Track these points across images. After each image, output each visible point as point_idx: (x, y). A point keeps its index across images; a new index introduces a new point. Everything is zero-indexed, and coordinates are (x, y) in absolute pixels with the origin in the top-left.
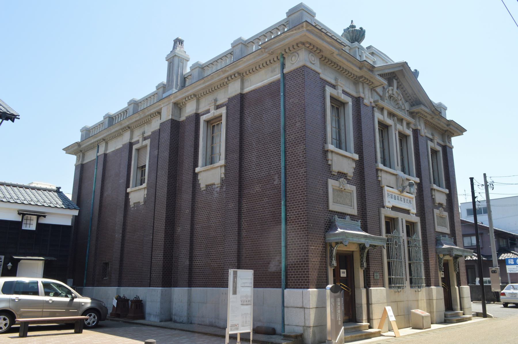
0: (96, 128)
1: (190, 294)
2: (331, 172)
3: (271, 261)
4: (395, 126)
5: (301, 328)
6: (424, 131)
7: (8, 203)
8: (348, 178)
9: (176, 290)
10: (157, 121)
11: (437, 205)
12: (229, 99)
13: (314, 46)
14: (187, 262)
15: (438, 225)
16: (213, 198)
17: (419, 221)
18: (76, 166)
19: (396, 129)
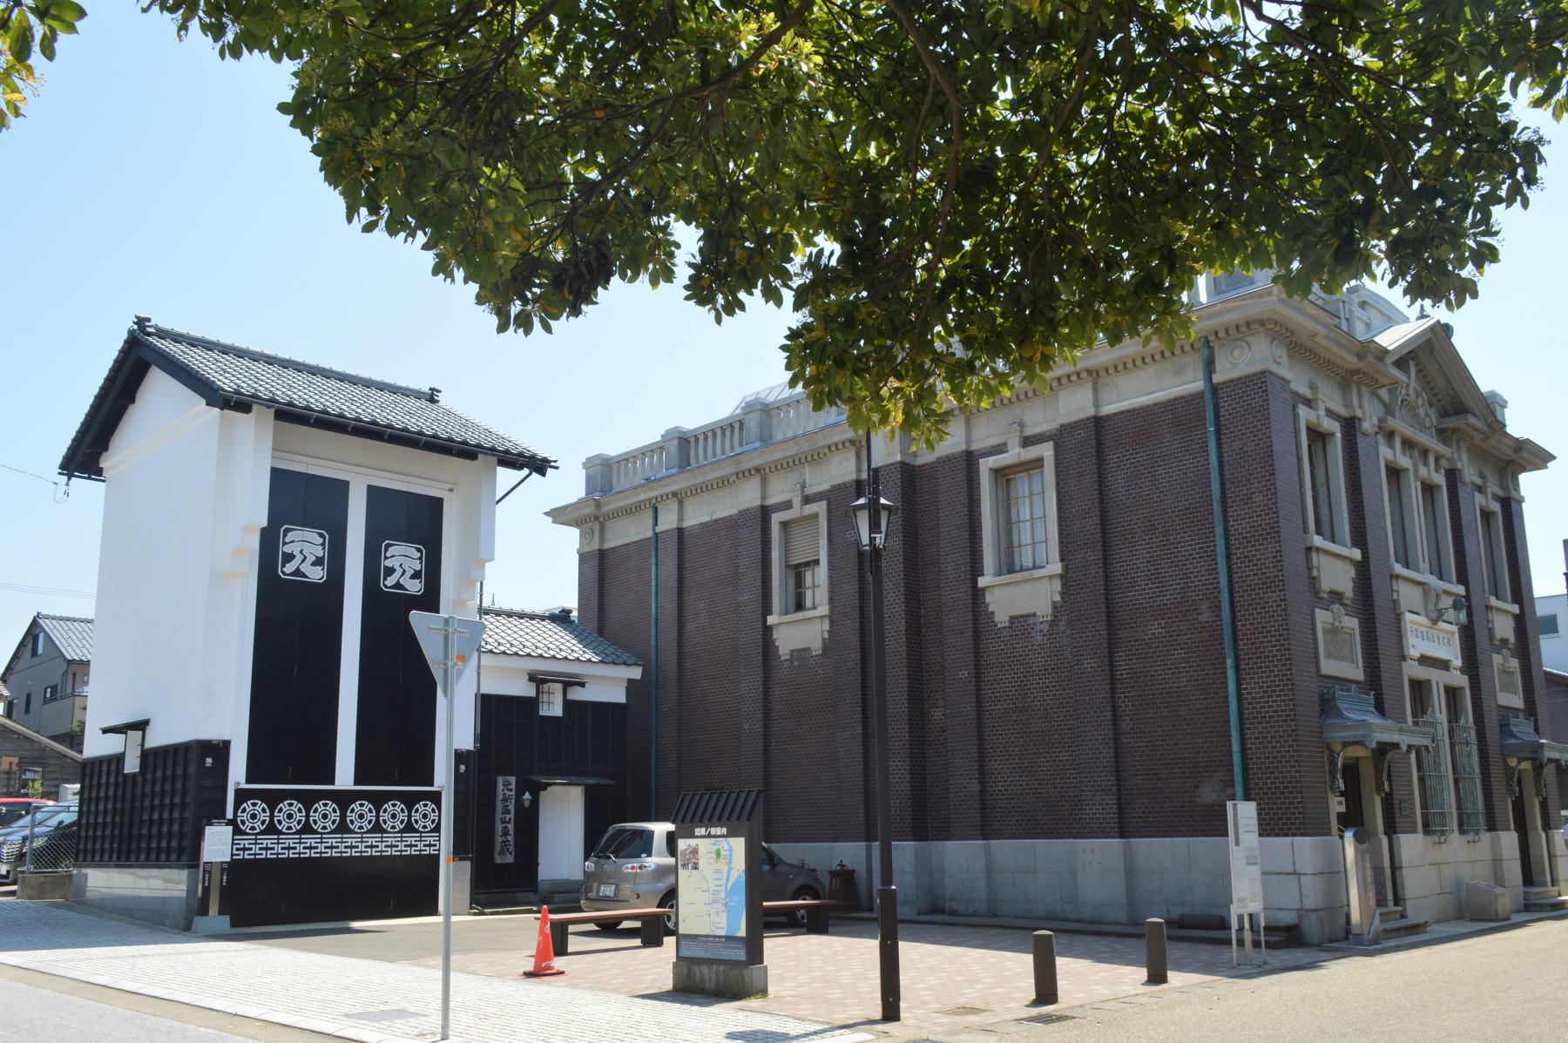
0: (631, 460)
1: (987, 850)
2: (1317, 593)
3: (1201, 782)
4: (1416, 469)
5: (1294, 914)
6: (1470, 474)
7: (515, 657)
8: (1345, 601)
9: (952, 846)
10: (848, 460)
11: (1497, 643)
12: (1062, 426)
13: (1281, 325)
14: (974, 786)
15: (1326, 657)
16: (1033, 646)
17: (1468, 685)
18: (584, 558)
19: (1416, 478)
